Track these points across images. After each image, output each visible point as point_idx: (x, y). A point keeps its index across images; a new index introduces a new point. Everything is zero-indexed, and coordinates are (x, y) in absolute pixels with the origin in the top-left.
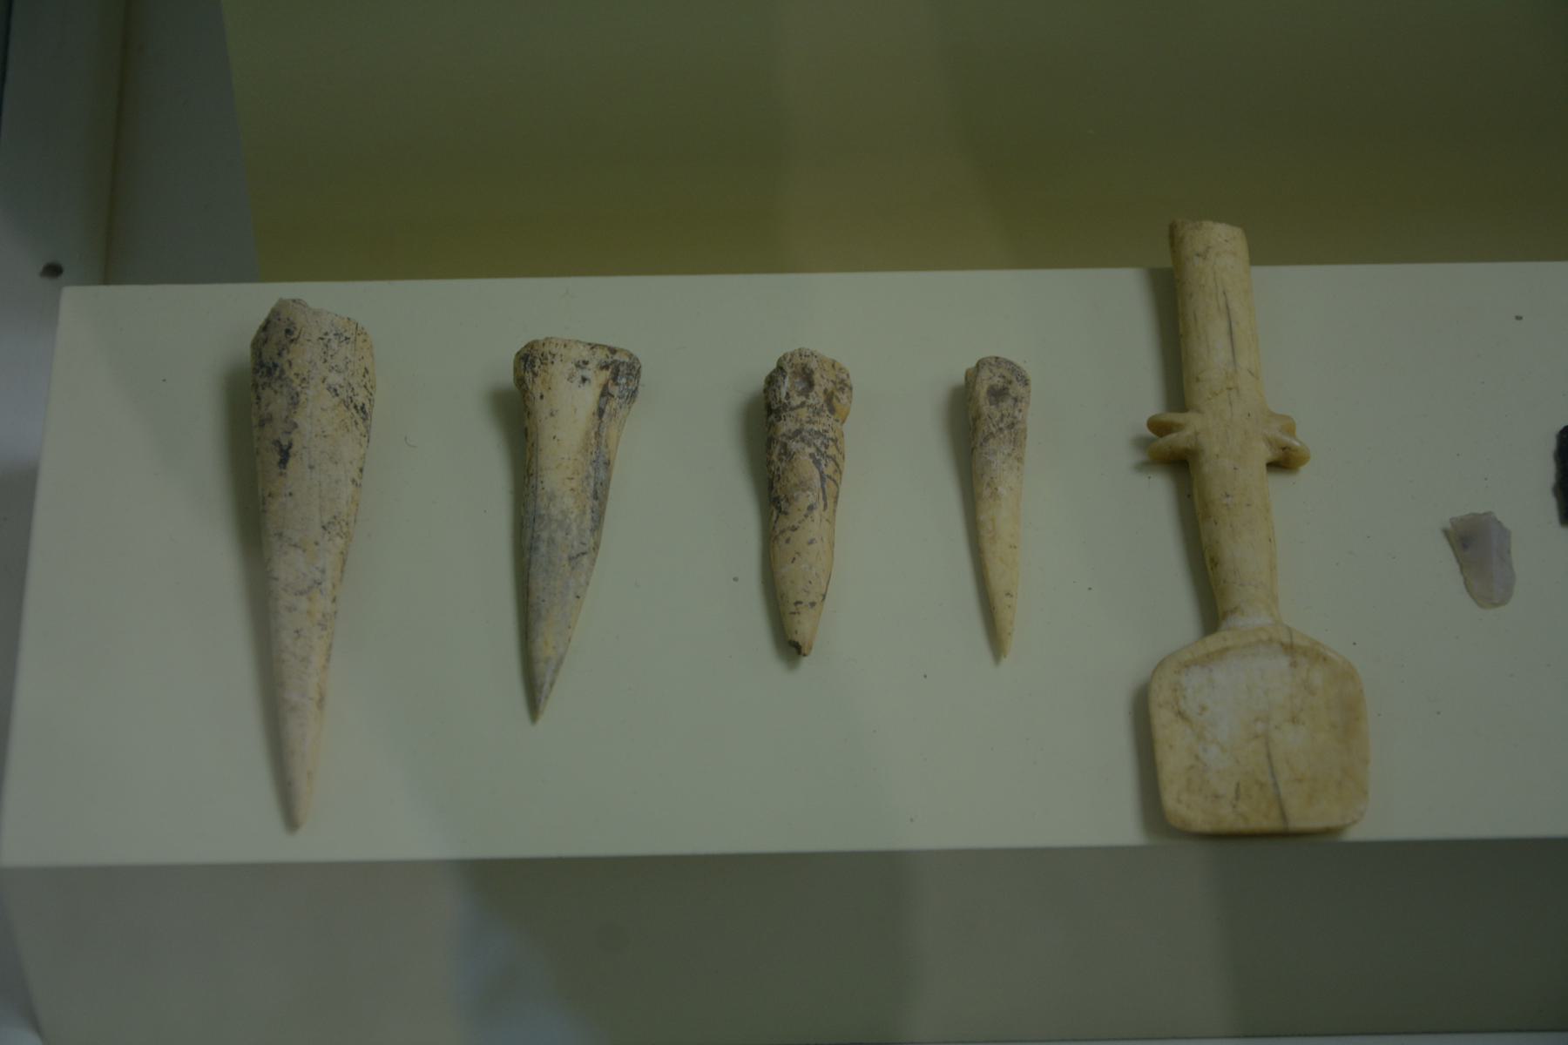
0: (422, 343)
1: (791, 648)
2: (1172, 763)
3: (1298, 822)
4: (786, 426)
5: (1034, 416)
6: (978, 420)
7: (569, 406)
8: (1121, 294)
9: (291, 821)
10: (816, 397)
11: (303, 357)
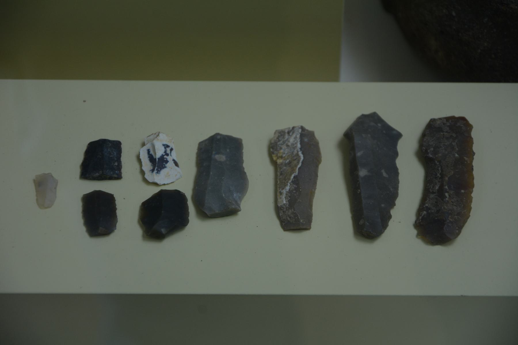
5: (83, 229)
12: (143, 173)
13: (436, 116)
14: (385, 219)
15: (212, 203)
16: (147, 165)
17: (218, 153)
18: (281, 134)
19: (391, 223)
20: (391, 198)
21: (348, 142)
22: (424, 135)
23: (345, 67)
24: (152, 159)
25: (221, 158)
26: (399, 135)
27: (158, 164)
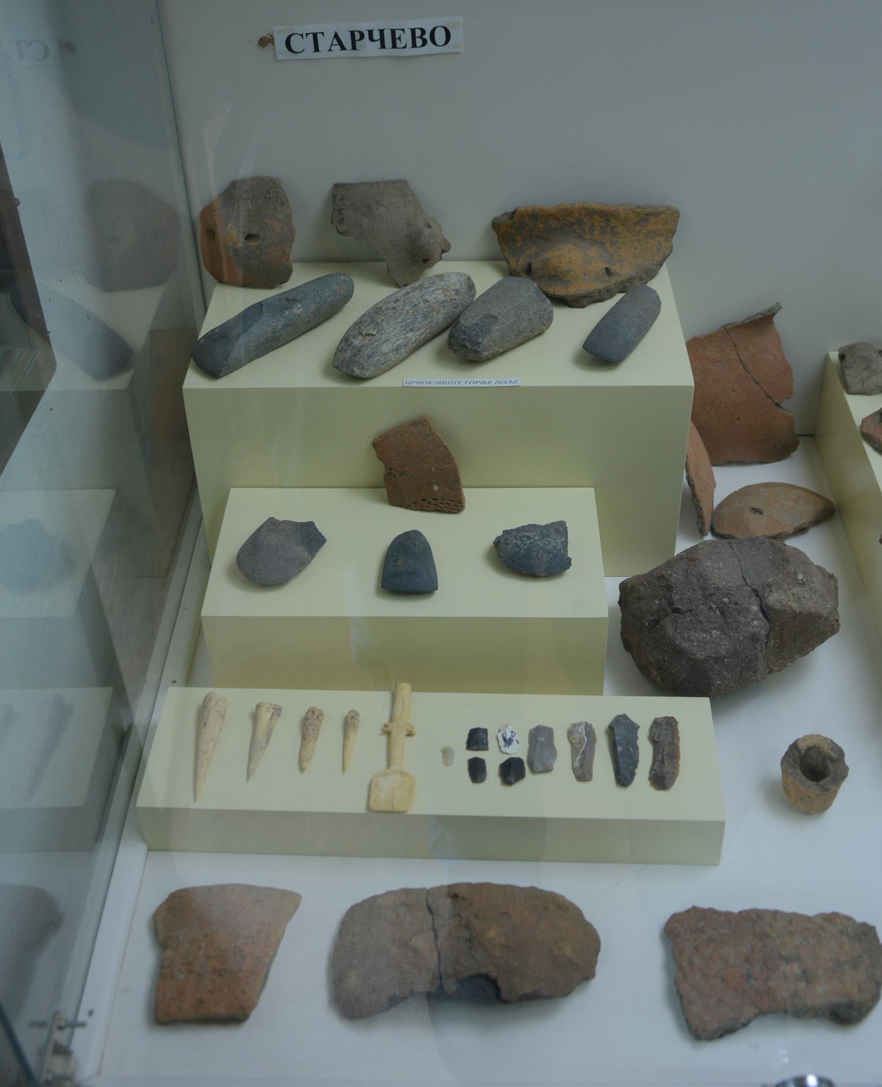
0: (237, 701)
1: (302, 769)
2: (373, 796)
3: (395, 810)
4: (308, 723)
5: (469, 779)
6: (350, 722)
7: (265, 716)
8: (386, 696)
9: (195, 800)
10: (315, 717)
11: (212, 705)
12: (500, 747)
13: (658, 716)
14: (632, 775)
15: (538, 765)
16: (502, 743)
17: (541, 736)
18: (574, 726)
19: (636, 777)
20: (635, 763)
21: (611, 730)
22: (652, 727)
23: (607, 687)
24: (505, 739)
25: (542, 739)
26: (638, 727)
27: (508, 742)
